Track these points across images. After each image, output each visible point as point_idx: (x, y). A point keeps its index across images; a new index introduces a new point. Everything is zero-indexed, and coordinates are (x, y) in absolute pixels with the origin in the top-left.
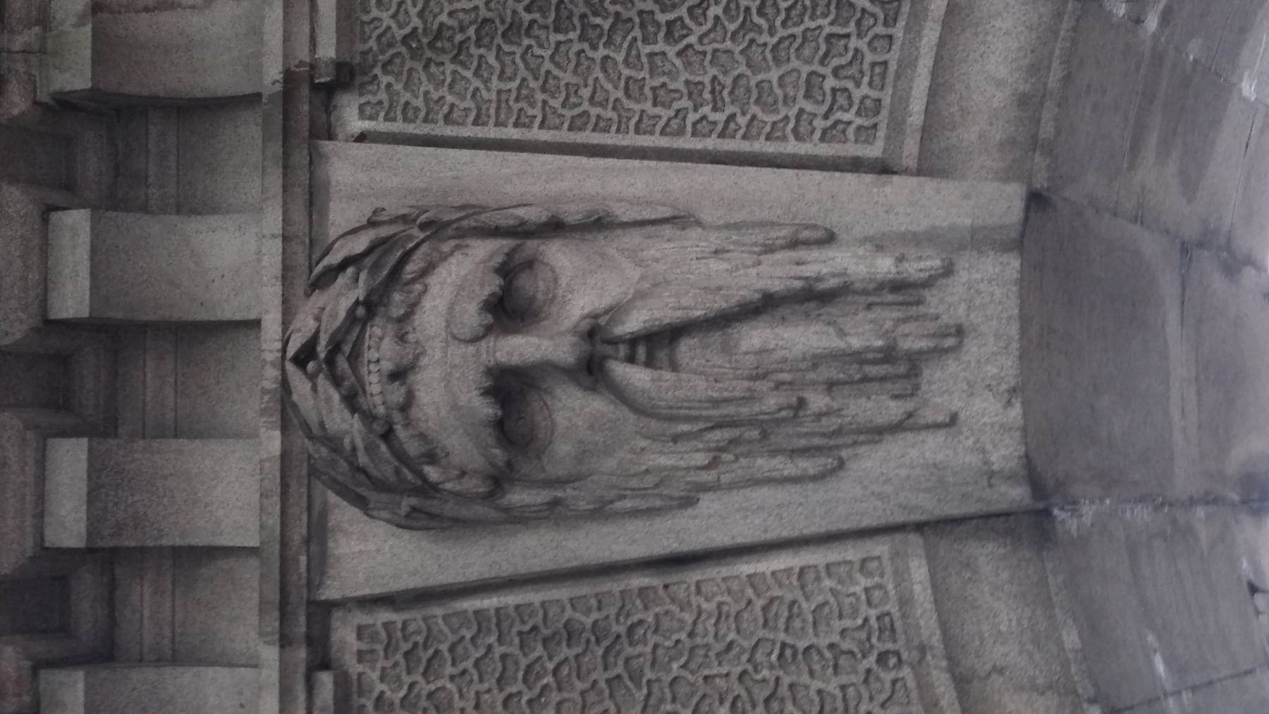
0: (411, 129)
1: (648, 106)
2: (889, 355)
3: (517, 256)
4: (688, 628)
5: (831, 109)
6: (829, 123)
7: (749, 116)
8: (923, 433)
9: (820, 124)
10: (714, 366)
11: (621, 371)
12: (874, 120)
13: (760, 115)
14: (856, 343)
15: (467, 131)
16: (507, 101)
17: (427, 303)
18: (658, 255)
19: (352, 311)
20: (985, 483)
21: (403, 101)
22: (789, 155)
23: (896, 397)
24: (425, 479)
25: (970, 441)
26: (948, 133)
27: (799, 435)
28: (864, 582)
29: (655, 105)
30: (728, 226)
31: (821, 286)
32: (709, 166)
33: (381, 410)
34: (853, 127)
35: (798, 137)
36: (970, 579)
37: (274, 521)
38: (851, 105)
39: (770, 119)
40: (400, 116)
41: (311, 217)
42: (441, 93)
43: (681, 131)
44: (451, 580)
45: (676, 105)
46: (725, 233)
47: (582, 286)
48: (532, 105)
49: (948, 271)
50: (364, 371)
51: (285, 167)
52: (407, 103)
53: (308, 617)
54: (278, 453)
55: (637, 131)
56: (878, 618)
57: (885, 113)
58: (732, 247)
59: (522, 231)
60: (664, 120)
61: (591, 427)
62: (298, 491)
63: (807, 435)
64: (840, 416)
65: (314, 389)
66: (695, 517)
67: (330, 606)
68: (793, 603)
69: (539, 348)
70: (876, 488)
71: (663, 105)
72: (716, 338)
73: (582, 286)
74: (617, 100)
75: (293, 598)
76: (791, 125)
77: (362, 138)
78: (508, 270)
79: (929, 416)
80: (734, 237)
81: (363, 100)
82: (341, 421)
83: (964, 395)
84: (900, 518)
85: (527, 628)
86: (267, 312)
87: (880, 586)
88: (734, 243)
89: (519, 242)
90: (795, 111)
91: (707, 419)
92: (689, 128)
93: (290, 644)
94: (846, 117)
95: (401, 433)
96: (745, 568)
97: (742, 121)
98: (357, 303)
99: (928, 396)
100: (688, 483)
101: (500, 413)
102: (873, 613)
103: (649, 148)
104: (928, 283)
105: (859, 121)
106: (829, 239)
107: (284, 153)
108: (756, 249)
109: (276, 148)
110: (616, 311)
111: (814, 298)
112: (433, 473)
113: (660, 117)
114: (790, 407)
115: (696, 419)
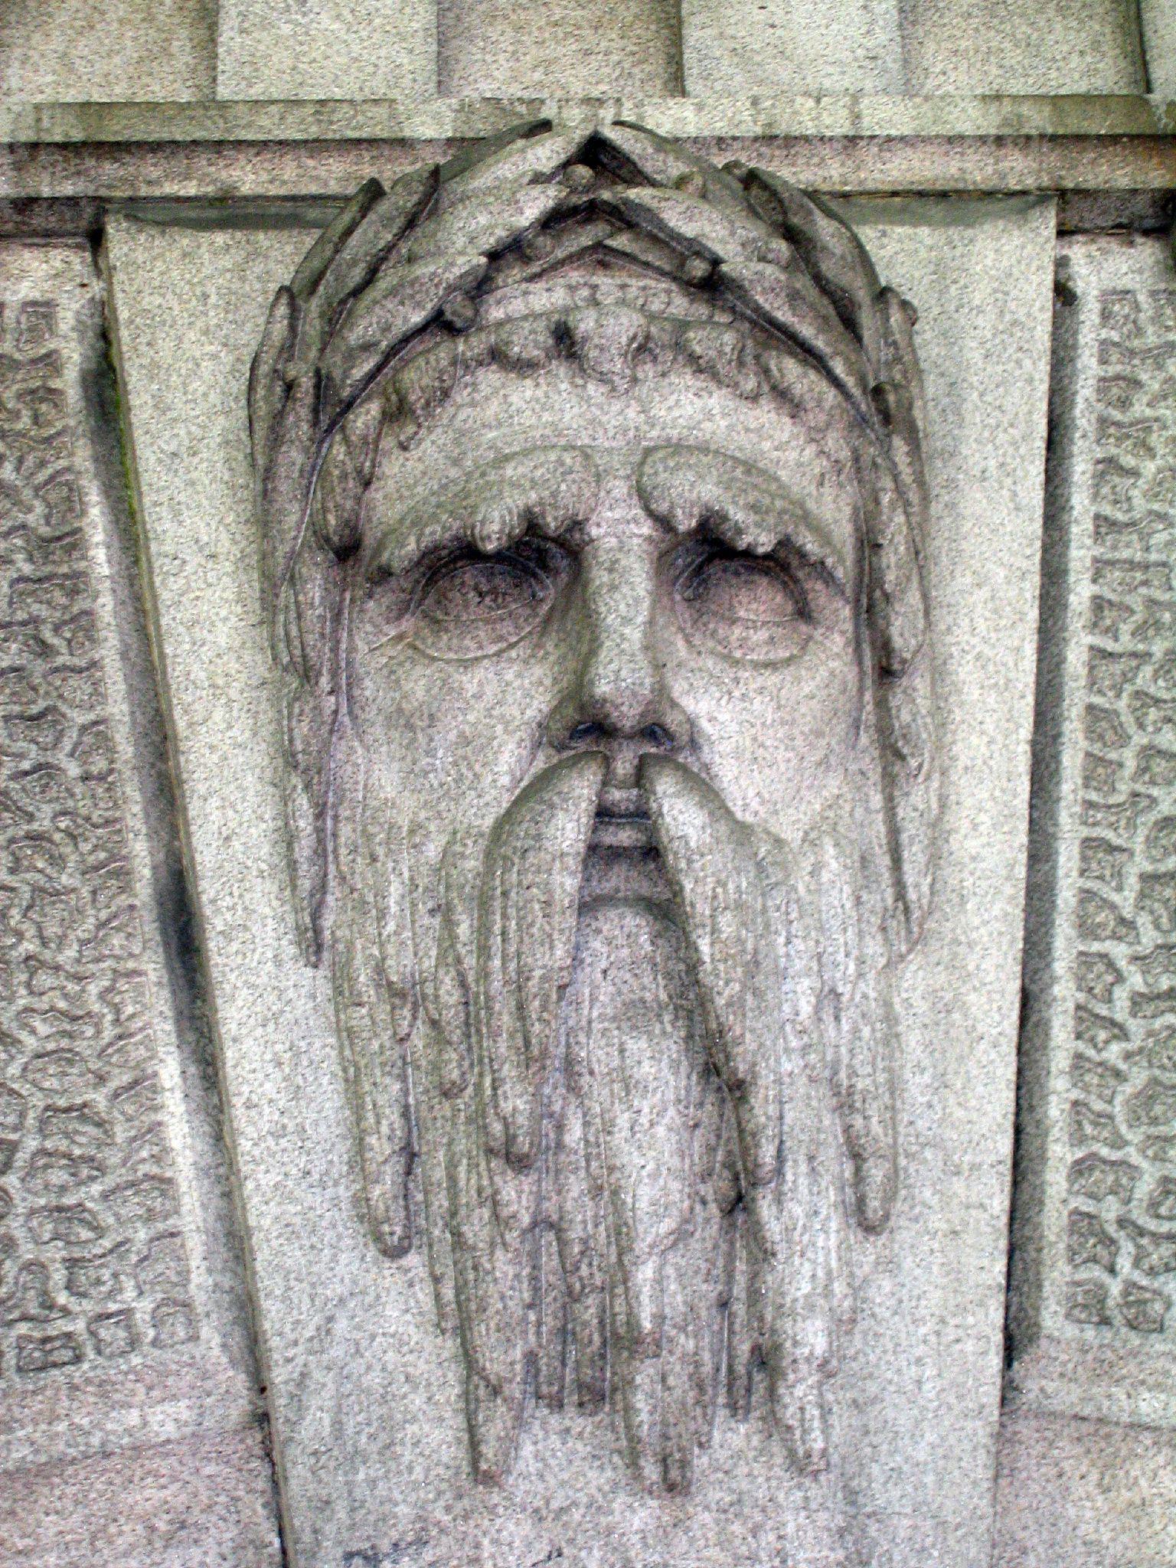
0: (1084, 392)
1: (1140, 863)
2: (624, 1341)
3: (819, 586)
4: (47, 955)
5: (1142, 1232)
6: (1111, 1229)
7: (1123, 1066)
8: (460, 1421)
9: (1110, 1210)
10: (595, 987)
11: (582, 789)
12: (1118, 1320)
13: (1128, 1089)
14: (645, 1274)
15: (1080, 502)
16: (1145, 583)
17: (718, 400)
18: (825, 876)
19: (696, 248)
20: (355, 1547)
21: (1144, 377)
22: (1043, 1149)
23: (531, 1358)
24: (349, 405)
25: (439, 1515)
26: (1094, 1476)
27: (452, 1165)
28: (143, 1308)
29: (1144, 878)
30: (890, 1018)
31: (765, 1209)
32: (1017, 985)
33: (496, 313)
34: (1106, 1278)
35: (1079, 1169)
36: (153, 1529)
37: (268, 126)
38: (1152, 1272)
39: (1118, 1109)
40: (1112, 370)
41: (895, 194)
42: (1161, 450)
43: (1086, 929)
44: (145, 478)
45: (1143, 920)
46: (875, 1009)
47: (755, 719)
48: (1139, 632)
49: (800, 1465)
50: (575, 276)
51: (999, 140)
52: (1137, 384)
53: (72, 201)
54: (407, 133)
55: (1087, 843)
56: (69, 1336)
57: (1135, 1340)
58: (846, 1026)
59: (870, 603)
60: (1115, 898)
61: (465, 740)
62: (335, 175)
63: (452, 1179)
64: (492, 1245)
65: (538, 179)
66: (278, 961)
67: (95, 239)
68: (102, 1169)
69: (627, 621)
70: (341, 1326)
71: (1142, 895)
72: (656, 990)
73: (755, 719)
74: (1154, 801)
75: (109, 169)
76: (1105, 1152)
77: (1064, 294)
78: (780, 565)
79: (495, 1425)
80: (866, 1032)
81: (1142, 298)
82: (468, 233)
83: (539, 1503)
84: (279, 1376)
85: (47, 635)
86: (700, 107)
87: (134, 1343)
88: (856, 1031)
89: (849, 592)
90: (1135, 1158)
91: (484, 974)
92: (1096, 947)
93: (18, 167)
94: (1124, 1264)
95: (443, 352)
96: (170, 1069)
97: (1114, 1053)
98: (716, 262)
99: (536, 1427)
100: (350, 947)
101: (490, 547)
102: (79, 1326)
103: (1054, 868)
104: (773, 1423)
105: (1115, 1288)
106: (865, 1219)
107: (1028, 138)
108: (843, 1074)
109: (1038, 120)
110: (704, 788)
111: (737, 1192)
112: (365, 417)
113: (1119, 889)
114: (510, 1139)
115: (484, 951)
